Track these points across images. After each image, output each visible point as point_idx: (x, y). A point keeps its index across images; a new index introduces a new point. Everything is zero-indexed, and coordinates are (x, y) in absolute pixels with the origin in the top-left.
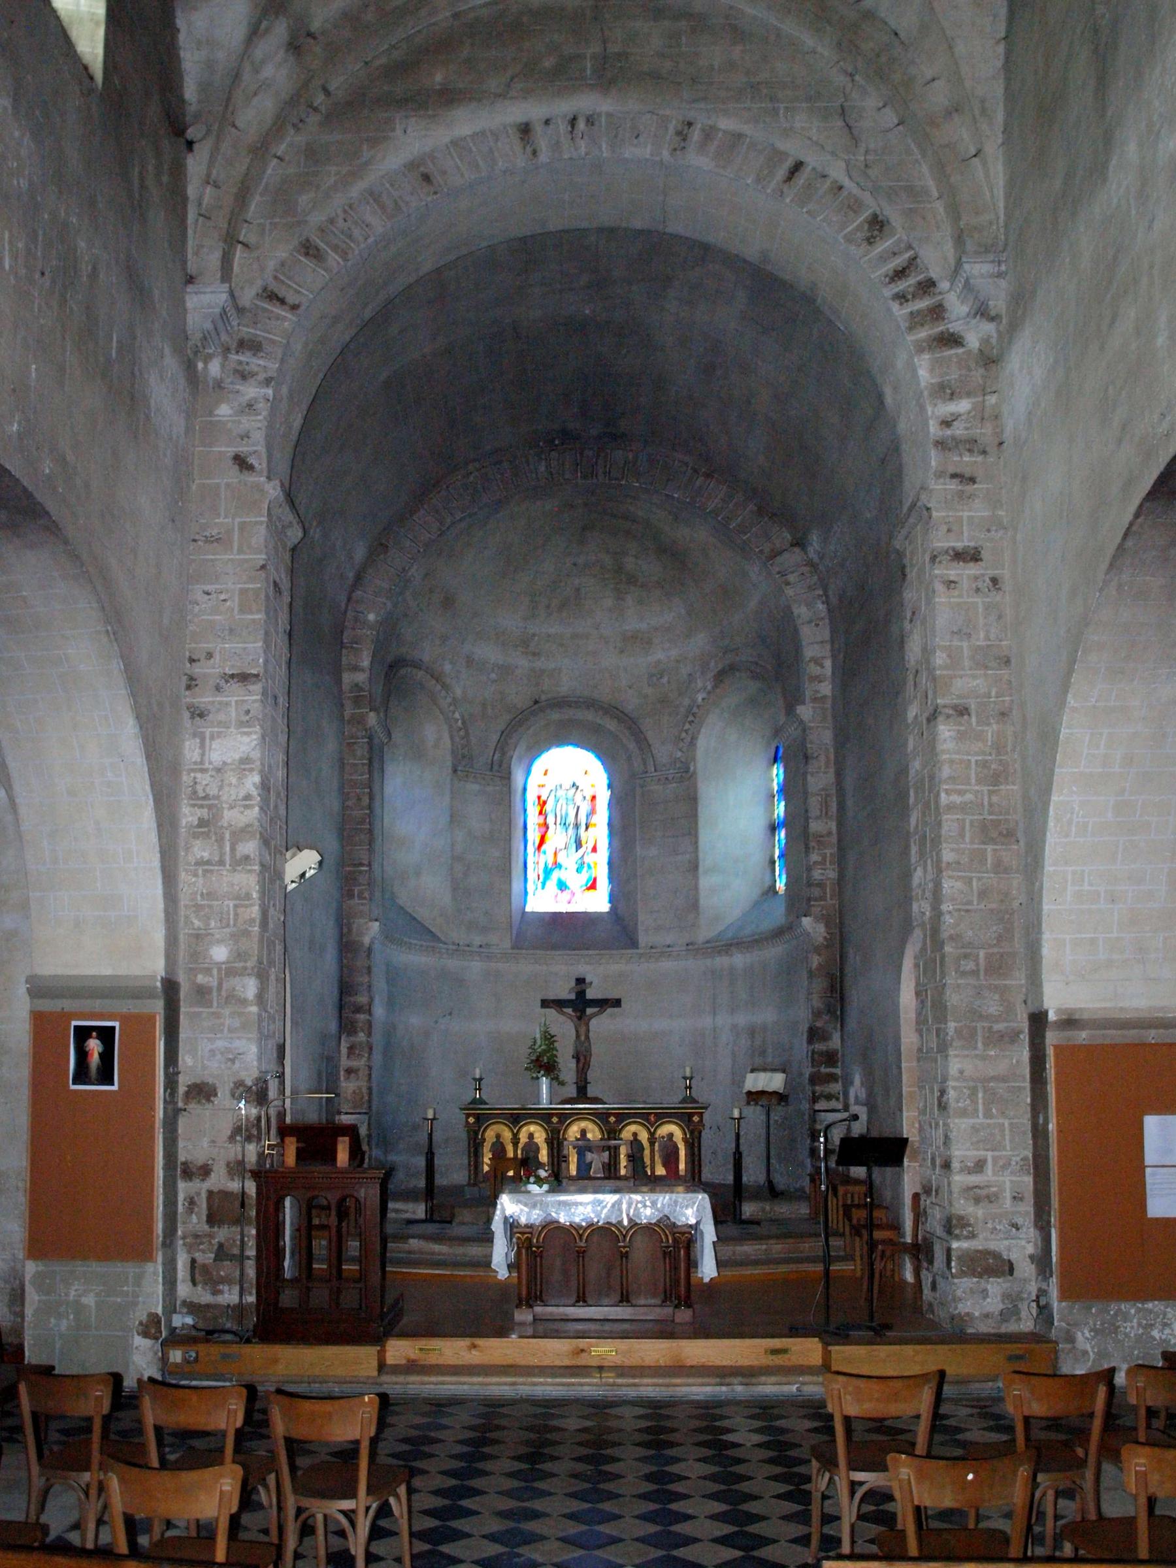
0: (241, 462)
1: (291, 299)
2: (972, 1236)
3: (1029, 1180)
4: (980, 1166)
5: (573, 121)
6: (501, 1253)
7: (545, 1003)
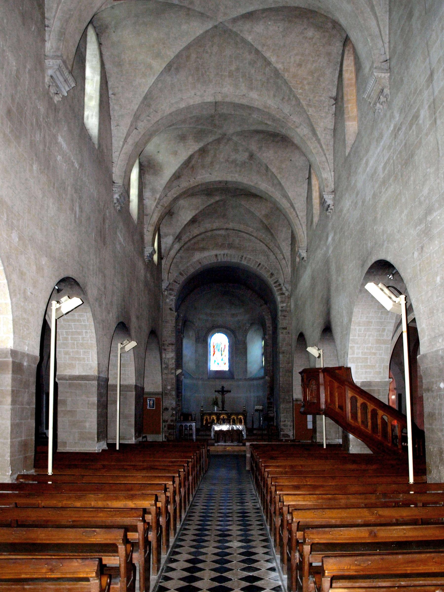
0: (171, 309)
1: (178, 282)
2: (284, 432)
3: (292, 423)
4: (285, 421)
5: (224, 255)
6: (212, 434)
7: (216, 391)
